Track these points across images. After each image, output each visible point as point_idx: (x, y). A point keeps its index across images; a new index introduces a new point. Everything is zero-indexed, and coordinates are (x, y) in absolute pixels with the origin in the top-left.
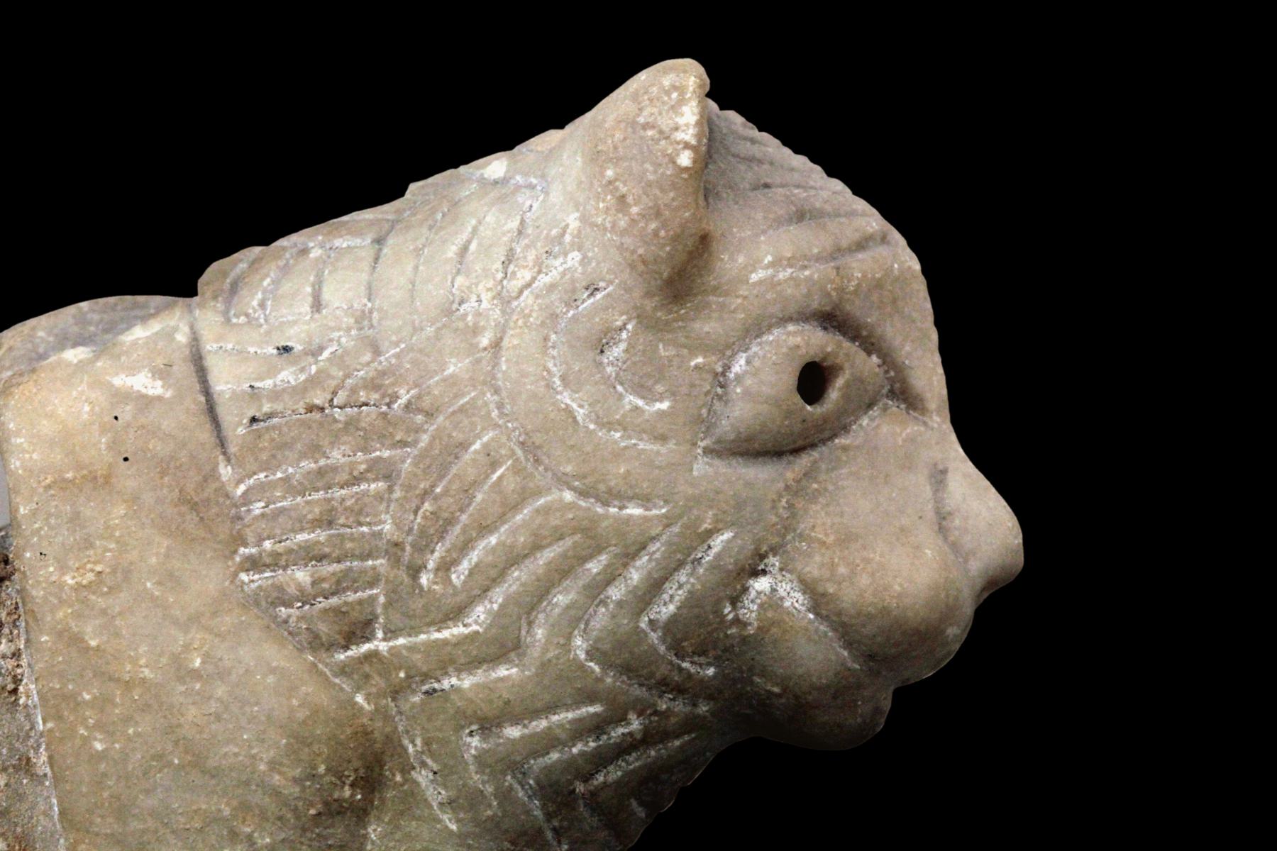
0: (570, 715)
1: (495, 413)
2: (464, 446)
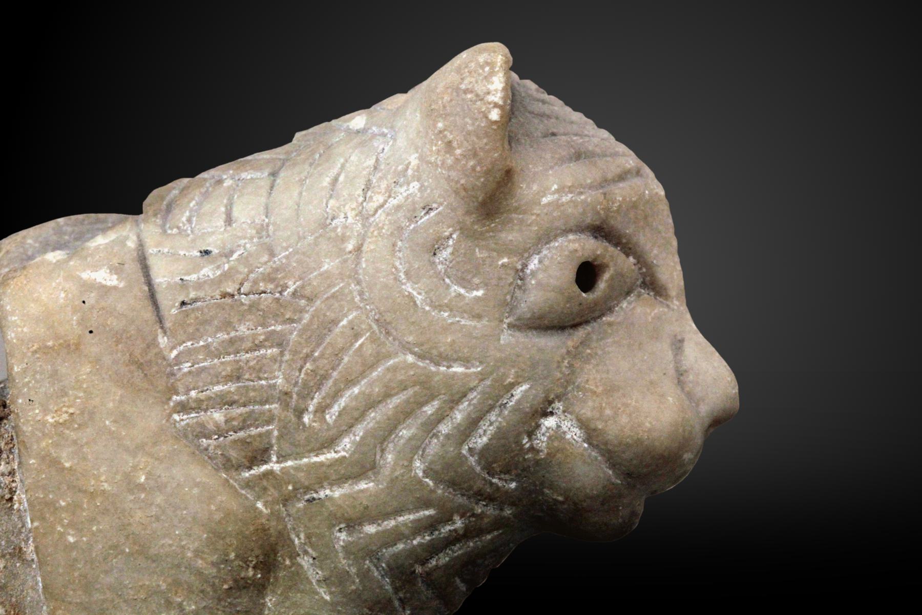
0: (412, 517)
1: (357, 299)
2: (335, 322)
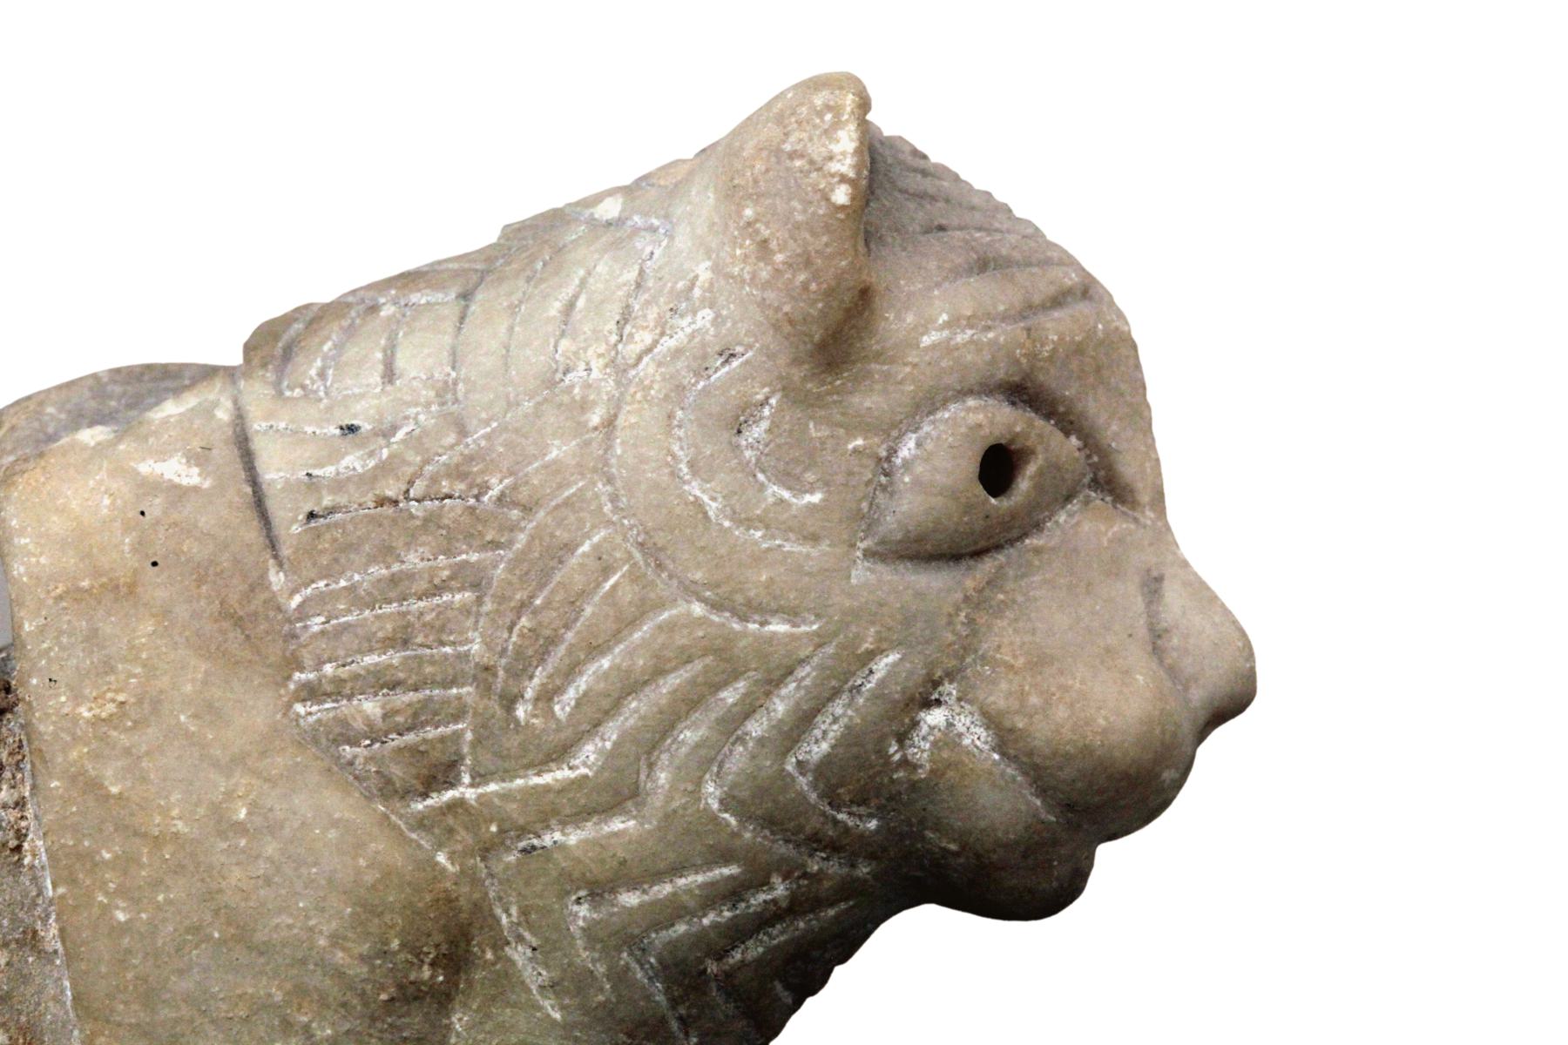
0: (700, 878)
1: (608, 508)
2: (570, 547)
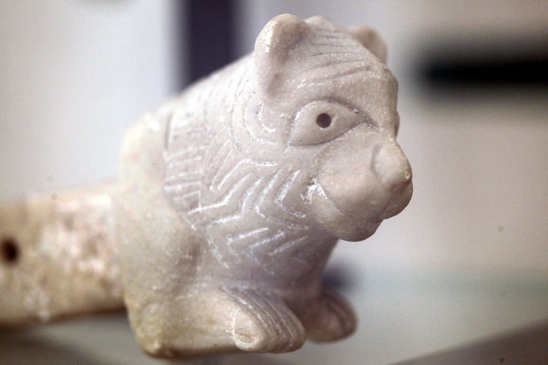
0: (258, 231)
1: (230, 134)
2: (221, 145)
